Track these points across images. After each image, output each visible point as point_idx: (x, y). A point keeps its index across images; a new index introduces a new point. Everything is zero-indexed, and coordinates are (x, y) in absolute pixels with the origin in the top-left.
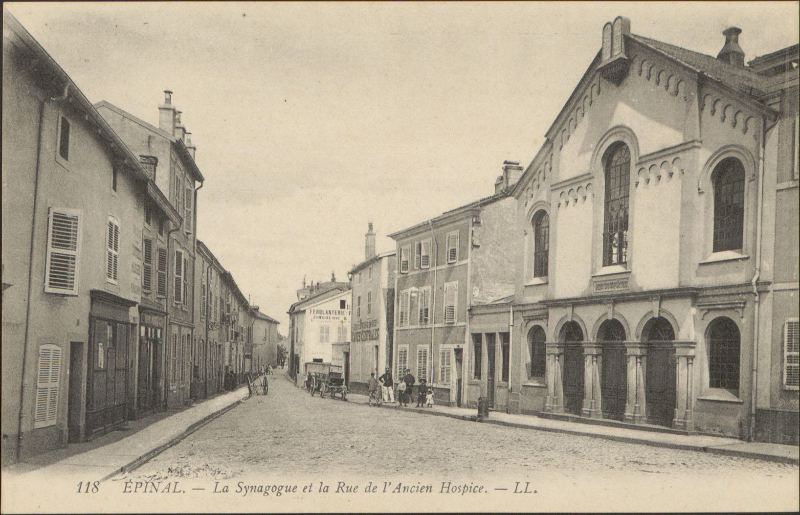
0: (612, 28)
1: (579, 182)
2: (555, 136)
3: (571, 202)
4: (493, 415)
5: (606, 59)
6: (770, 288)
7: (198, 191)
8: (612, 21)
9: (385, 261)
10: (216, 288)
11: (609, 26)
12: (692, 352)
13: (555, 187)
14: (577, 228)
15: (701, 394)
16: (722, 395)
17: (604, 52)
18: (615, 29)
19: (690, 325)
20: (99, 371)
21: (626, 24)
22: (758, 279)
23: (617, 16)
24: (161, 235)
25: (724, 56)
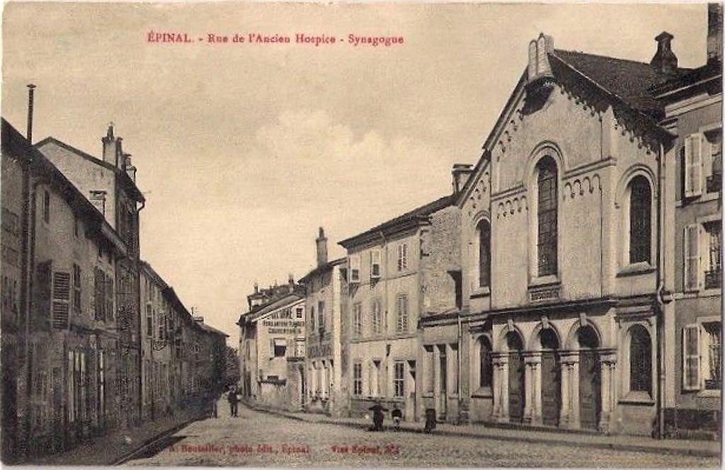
0: (537, 46)
1: (500, 198)
2: (493, 147)
3: (509, 214)
4: (439, 427)
5: (532, 75)
6: (671, 297)
7: (140, 212)
8: (536, 38)
9: (336, 270)
10: (160, 307)
11: (534, 44)
12: (612, 358)
13: (495, 196)
14: (516, 238)
15: (473, 393)
16: (641, 397)
17: (530, 69)
18: (539, 46)
19: (610, 329)
20: (417, 222)
21: (549, 41)
22: (663, 289)
23: (530, 40)
24: (101, 256)
25: (658, 58)
